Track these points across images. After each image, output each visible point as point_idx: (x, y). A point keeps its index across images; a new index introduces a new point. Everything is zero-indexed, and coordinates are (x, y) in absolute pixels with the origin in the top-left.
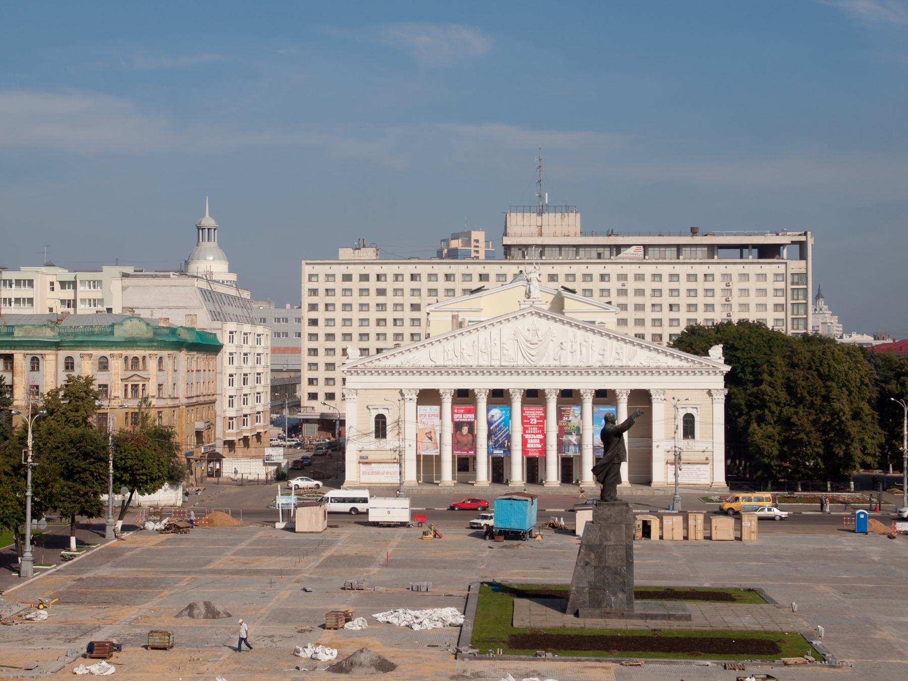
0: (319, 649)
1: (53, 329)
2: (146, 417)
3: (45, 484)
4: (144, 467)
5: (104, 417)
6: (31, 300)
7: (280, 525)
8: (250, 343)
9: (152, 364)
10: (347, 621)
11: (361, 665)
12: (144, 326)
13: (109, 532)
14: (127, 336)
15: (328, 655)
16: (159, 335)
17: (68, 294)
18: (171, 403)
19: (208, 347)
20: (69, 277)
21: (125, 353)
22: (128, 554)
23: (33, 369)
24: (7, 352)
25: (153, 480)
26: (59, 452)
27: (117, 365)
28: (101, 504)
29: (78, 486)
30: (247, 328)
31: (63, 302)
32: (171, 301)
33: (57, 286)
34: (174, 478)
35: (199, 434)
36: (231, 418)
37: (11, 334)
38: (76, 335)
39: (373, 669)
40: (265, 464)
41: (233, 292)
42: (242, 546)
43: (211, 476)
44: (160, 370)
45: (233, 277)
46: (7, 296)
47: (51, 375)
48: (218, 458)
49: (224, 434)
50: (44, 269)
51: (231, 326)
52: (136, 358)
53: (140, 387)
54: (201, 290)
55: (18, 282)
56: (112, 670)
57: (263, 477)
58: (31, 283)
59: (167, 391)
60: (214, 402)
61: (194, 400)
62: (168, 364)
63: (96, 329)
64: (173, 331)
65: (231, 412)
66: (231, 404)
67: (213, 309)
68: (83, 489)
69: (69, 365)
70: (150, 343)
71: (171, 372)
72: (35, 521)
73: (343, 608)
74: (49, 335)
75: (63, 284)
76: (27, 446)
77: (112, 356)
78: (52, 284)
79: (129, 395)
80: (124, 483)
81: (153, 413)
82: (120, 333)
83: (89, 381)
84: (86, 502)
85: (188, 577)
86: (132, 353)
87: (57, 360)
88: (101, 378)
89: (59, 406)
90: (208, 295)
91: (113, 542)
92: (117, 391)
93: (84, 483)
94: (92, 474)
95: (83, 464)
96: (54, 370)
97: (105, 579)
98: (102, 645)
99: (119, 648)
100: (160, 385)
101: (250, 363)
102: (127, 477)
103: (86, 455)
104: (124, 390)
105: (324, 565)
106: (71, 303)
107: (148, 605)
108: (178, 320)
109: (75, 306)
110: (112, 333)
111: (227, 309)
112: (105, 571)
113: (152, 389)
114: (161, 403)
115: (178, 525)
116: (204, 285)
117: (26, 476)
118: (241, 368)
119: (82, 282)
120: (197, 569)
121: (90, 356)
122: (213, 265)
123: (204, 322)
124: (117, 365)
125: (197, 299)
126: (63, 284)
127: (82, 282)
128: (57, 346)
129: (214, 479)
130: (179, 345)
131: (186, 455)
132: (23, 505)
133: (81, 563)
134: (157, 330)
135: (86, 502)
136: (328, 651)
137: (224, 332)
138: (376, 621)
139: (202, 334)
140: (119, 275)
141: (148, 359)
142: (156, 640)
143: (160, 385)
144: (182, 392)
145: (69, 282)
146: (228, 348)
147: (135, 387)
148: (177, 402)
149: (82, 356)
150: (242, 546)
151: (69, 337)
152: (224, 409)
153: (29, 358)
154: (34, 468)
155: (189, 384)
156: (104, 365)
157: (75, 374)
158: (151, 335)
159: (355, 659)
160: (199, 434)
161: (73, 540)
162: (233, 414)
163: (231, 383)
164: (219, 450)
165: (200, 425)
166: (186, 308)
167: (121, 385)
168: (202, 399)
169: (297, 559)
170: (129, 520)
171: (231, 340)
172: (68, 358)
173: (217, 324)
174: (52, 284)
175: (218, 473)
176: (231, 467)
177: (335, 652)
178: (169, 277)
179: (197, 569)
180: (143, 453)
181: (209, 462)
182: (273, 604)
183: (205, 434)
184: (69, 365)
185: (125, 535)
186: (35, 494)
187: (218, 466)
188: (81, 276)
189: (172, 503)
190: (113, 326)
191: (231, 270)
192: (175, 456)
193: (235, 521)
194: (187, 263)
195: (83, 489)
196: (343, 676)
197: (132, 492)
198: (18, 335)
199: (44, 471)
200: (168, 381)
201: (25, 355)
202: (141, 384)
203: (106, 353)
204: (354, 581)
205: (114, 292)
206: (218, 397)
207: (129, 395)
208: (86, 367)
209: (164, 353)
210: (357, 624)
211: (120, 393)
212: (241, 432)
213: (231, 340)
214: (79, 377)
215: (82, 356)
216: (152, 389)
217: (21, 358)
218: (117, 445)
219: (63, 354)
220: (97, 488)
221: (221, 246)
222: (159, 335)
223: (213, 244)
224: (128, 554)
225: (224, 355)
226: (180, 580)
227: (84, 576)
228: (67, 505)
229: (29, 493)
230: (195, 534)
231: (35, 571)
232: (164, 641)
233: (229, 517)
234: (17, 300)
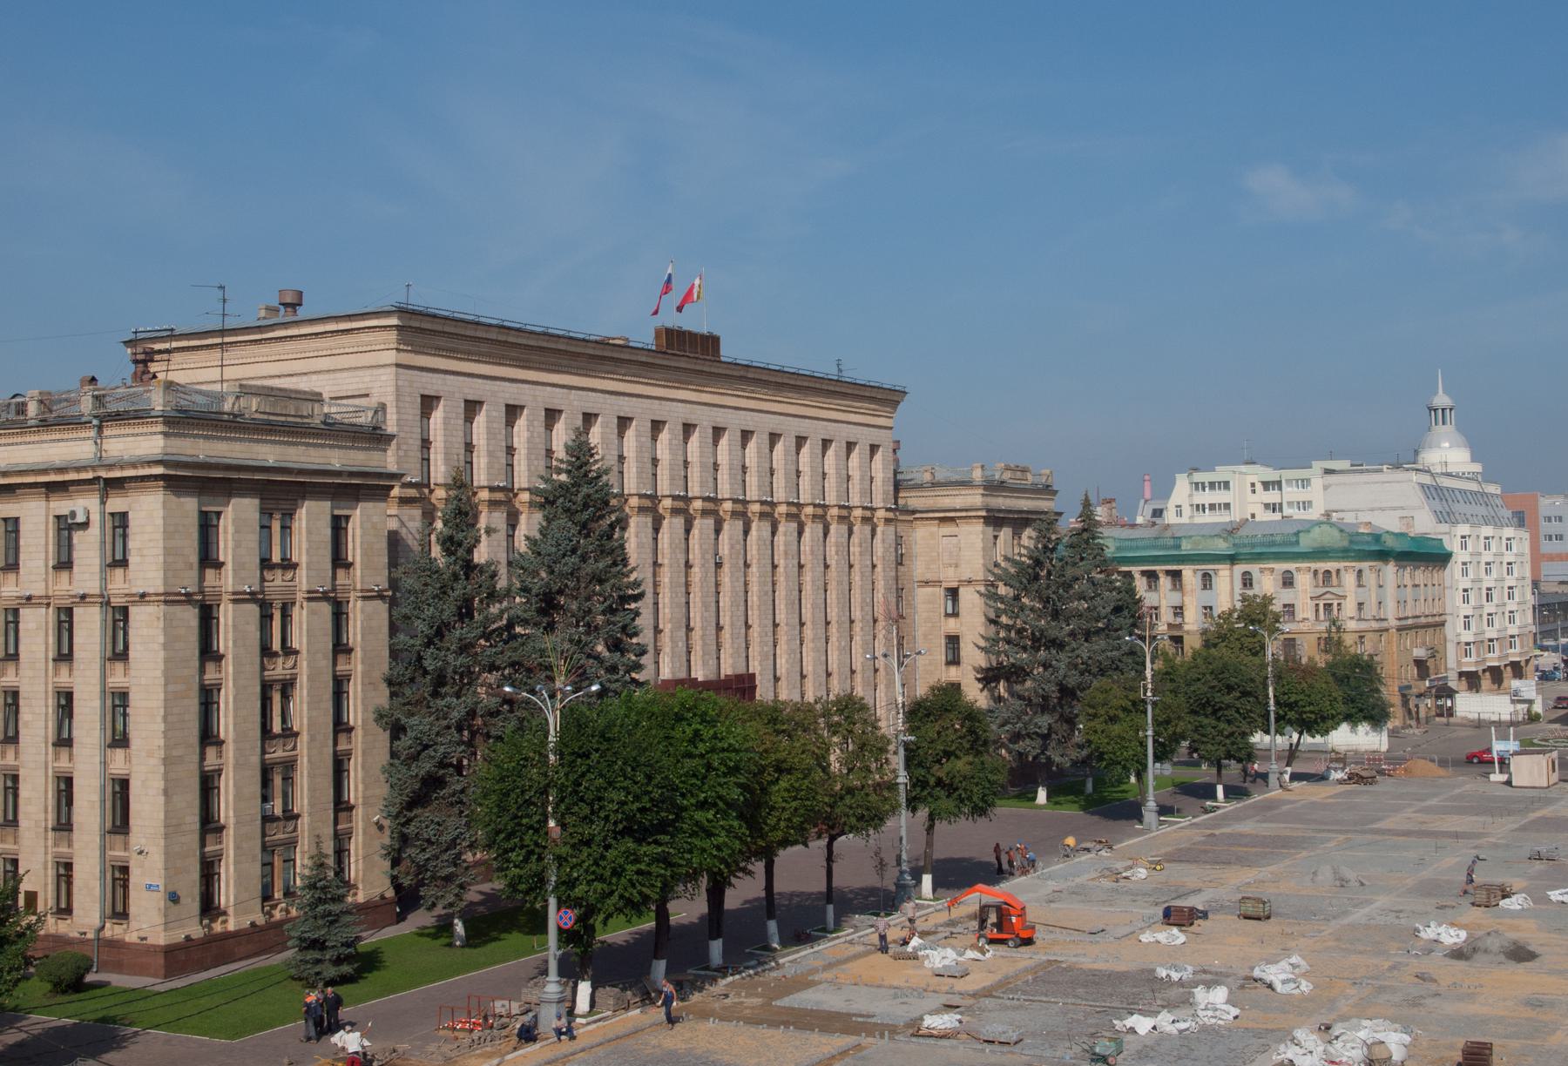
0: (1442, 930)
1: (1225, 540)
2: (1339, 642)
3: (1168, 722)
4: (1311, 704)
5: (1290, 644)
6: (1227, 506)
7: (1497, 777)
8: (1494, 549)
9: (1349, 579)
10: (1504, 897)
11: (1486, 951)
12: (1336, 533)
13: (1273, 779)
14: (1315, 545)
15: (1452, 937)
16: (1357, 543)
17: (1272, 496)
18: (1375, 625)
19: (1431, 557)
20: (1271, 475)
21: (1314, 566)
22: (1285, 808)
23: (1205, 587)
24: (1175, 568)
25: (1324, 719)
26: (1199, 684)
27: (1304, 581)
28: (1251, 746)
29: (1222, 725)
30: (1487, 531)
31: (1267, 506)
32: (1386, 502)
33: (1259, 487)
34: (1375, 716)
35: (1420, 664)
36: (1468, 644)
37: (1178, 547)
38: (1253, 546)
39: (1502, 958)
40: (1513, 702)
41: (1474, 487)
42: (1434, 802)
43: (1441, 715)
44: (1360, 586)
45: (1477, 468)
46: (1200, 502)
47: (1226, 592)
48: (1451, 694)
49: (1459, 663)
50: (1244, 468)
51: (1463, 529)
52: (1328, 572)
53: (1335, 607)
54: (1422, 486)
55: (1212, 485)
56: (1182, 938)
57: (1506, 717)
58: (1226, 485)
59: (1370, 610)
60: (1442, 624)
61: (1410, 622)
62: (1370, 578)
63: (1278, 539)
64: (1377, 538)
65: (1467, 636)
66: (1467, 626)
67: (1439, 508)
68: (1228, 729)
69: (1247, 581)
70: (1345, 554)
71: (1374, 588)
72: (1158, 765)
73: (1498, 880)
74: (1222, 546)
75: (1266, 485)
76: (1145, 679)
77: (1298, 569)
78: (1253, 485)
79: (1322, 617)
80: (1290, 722)
81: (1349, 640)
82: (1306, 543)
83: (1267, 600)
84: (1233, 743)
85: (1341, 837)
86: (1323, 566)
87: (1232, 576)
88: (1283, 597)
89: (1232, 630)
90: (1434, 492)
91: (1276, 793)
92: (1305, 610)
93: (1229, 722)
94: (1238, 711)
95: (1228, 699)
96: (1228, 588)
97: (1242, 835)
98: (1180, 910)
99: (1205, 915)
100: (1360, 604)
101: (1494, 575)
102: (1292, 715)
103: (1230, 688)
104: (1311, 610)
105: (1523, 829)
106: (1274, 507)
107: (1271, 868)
108: (1389, 523)
109: (1281, 510)
110: (1297, 543)
111: (1457, 507)
112: (1247, 827)
113: (1349, 608)
114: (1363, 626)
115: (1365, 771)
116: (1427, 479)
117: (1145, 712)
118: (1480, 581)
119: (1289, 482)
120: (1358, 828)
121: (1272, 570)
122: (1449, 454)
123: (1424, 523)
124: (1304, 581)
125: (1417, 498)
126: (1266, 485)
127: (1289, 482)
128: (1232, 559)
129: (1444, 720)
130: (1383, 555)
131: (1401, 689)
132: (1143, 744)
133: (1225, 817)
134: (1354, 537)
135: (1233, 743)
136: (1452, 932)
137: (1452, 538)
138: (917, 875)
139: (1422, 539)
140: (1321, 472)
141: (1342, 572)
142: (1249, 908)
143: (1360, 604)
144: (1391, 612)
145: (1273, 483)
146: (1460, 556)
147: (1328, 607)
148: (1384, 625)
149: (1262, 571)
150: (1434, 802)
151: (1244, 548)
152: (1456, 631)
153: (1200, 574)
154: (1154, 704)
155: (1401, 603)
156: (1288, 581)
157: (1250, 593)
158: (1345, 543)
159: (1480, 944)
160: (1420, 664)
161: (1220, 789)
162: (1494, 635)
163: (1466, 600)
164: (1453, 684)
165: (1420, 653)
166: (1402, 508)
167: (1311, 604)
168: (1423, 620)
169: (1490, 819)
170: (1299, 767)
171: (1464, 546)
172: (1246, 573)
173: (1444, 527)
174: (1253, 485)
175: (1451, 712)
176: (1468, 705)
177: (1463, 934)
178: (1381, 471)
179: (1358, 828)
180: (1311, 686)
181: (1438, 697)
182: (1426, 874)
183: (1430, 663)
184: (1247, 581)
185: (1295, 784)
186: (1157, 734)
187: (1449, 703)
188: (1287, 474)
189: (1375, 747)
190: (1297, 534)
191: (1474, 460)
192: (1378, 691)
193: (1442, 772)
194: (1416, 453)
195: (1228, 729)
196: (1461, 964)
197: (1301, 733)
198: (1187, 547)
199: (1167, 707)
200: (1369, 601)
201: (1195, 571)
202: (1335, 603)
203: (1291, 566)
204: (1543, 849)
205: (1324, 496)
206: (1448, 618)
207: (1322, 617)
208: (1267, 583)
209: (1365, 565)
210: (1513, 903)
211: (1310, 615)
212: (1484, 660)
213: (1464, 546)
214: (1255, 596)
215: (1262, 571)
216: (1349, 608)
217: (1189, 574)
218: (1278, 677)
219: (1240, 569)
220: (1245, 727)
221: (1459, 429)
222: (1357, 543)
223: (1449, 428)
224: (1285, 808)
225: (1454, 568)
226: (1329, 840)
227: (1217, 832)
228: (1209, 747)
229: (1150, 733)
230: (1384, 785)
231: (1162, 823)
232: (1259, 910)
233: (1434, 766)
234: (1212, 507)
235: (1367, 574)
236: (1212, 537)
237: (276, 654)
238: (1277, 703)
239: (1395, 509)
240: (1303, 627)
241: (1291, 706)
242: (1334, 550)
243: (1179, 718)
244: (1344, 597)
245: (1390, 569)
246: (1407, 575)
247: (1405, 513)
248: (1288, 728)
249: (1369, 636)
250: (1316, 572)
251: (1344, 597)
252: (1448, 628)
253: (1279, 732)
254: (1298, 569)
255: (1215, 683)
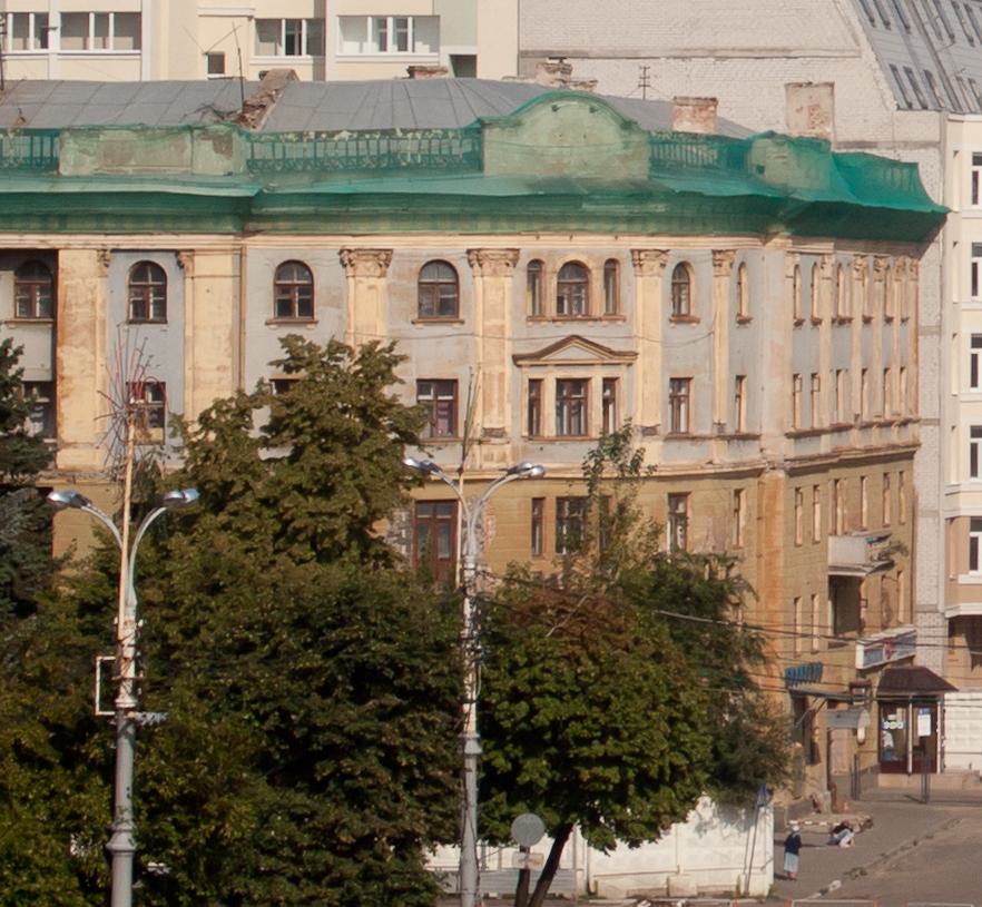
1: (223, 145)
2: (620, 519)
3: (193, 802)
4: (609, 732)
9: (646, 294)
12: (610, 134)
14: (539, 172)
16: (676, 169)
18: (723, 456)
21: (531, 244)
23: (139, 314)
24: (32, 241)
25: (647, 784)
27: (494, 297)
29: (331, 812)
35: (843, 589)
38: (321, 168)
44: (680, 318)
47: (220, 339)
52: (576, 268)
60: (907, 454)
61: (824, 445)
62: (712, 293)
63: (409, 146)
64: (734, 152)
67: (903, 60)
68: (354, 824)
69: (295, 295)
70: (634, 204)
71: (724, 326)
74: (209, 168)
76: (113, 641)
79: (549, 424)
80: (528, 796)
81: (649, 501)
82: (508, 162)
83: (378, 364)
84: (367, 876)
86: (559, 246)
87: (240, 276)
88: (428, 352)
89: (250, 469)
92: (496, 405)
93: (357, 799)
94: (389, 760)
95: (352, 717)
100: (678, 383)
102: (537, 770)
108: (755, 105)
109: (317, 47)
110: (475, 162)
113: (643, 400)
114: (685, 458)
117: (108, 770)
121: (384, 258)
128: (244, 215)
129: (909, 783)
130: (760, 214)
134: (664, 149)
135: (367, 876)
139: (855, 164)
141: (626, 270)
143: (678, 383)
144: (770, 411)
147: (573, 389)
148: (749, 455)
149: (347, 259)
153: (123, 265)
154: (143, 735)
155: (802, 379)
156: (439, 297)
158: (638, 170)
160: (843, 589)
165: (848, 552)
166: (786, 54)
167: (515, 381)
168: (856, 441)
180: (608, 670)
181: (887, 707)
183: (869, 590)
184: (295, 295)
186: (149, 844)
189: (728, 880)
190: (477, 130)
192: (743, 681)
195: (354, 824)
197: (560, 835)
198: (78, 167)
199: (186, 746)
201: (105, 256)
202: (597, 377)
203: (449, 244)
206: (924, 434)
207: (549, 424)
208: (363, 306)
209: (697, 247)
214: (336, 348)
215: (347, 259)
216: (643, 400)
217: (88, 269)
219: (268, 250)
220: (413, 818)
222: (676, 169)
229: (123, 841)
235: (703, 277)
236: (171, 132)
237: (168, 659)
238: (488, 728)
239: (759, 55)
240: (487, 460)
241: (531, 740)
242: (598, 193)
243: (233, 786)
244: (628, 358)
245: (774, 257)
246: (824, 288)
247: (797, 71)
248: (527, 820)
249: (701, 494)
250: (535, 267)
251: (628, 358)
252: (922, 470)
253: (493, 834)
254: (475, 257)
255: (314, 659)
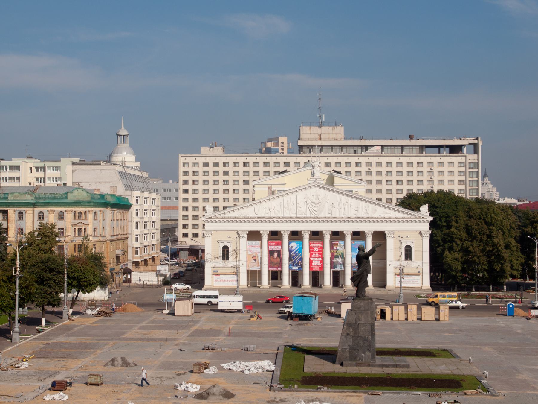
0: (189, 385)
1: (31, 195)
2: (87, 247)
3: (27, 287)
4: (85, 277)
5: (61, 248)
6: (18, 178)
7: (166, 311)
8: (148, 203)
9: (90, 216)
10: (206, 368)
11: (214, 394)
12: (85, 194)
13: (65, 315)
14: (75, 199)
15: (194, 389)
16: (94, 199)
17: (40, 175)
18: (101, 239)
19: (123, 206)
20: (41, 164)
21: (74, 209)
22: (76, 329)
23: (19, 219)
24: (4, 209)
25: (90, 285)
26: (35, 268)
27: (69, 217)
28: (60, 299)
29: (46, 289)
30: (146, 195)
31: (37, 179)
32: (101, 179)
33: (34, 169)
34: (103, 284)
35: (118, 257)
36: (137, 248)
37: (7, 198)
38: (45, 199)
39: (221, 397)
40: (157, 275)
41: (138, 173)
42: (143, 324)
43: (125, 282)
44: (95, 219)
45: (138, 164)
46: (4, 176)
47: (30, 222)
48: (129, 272)
49: (133, 257)
50: (26, 160)
51: (137, 193)
52: (81, 212)
53: (83, 230)
54: (119, 172)
55: (11, 167)
56: (67, 397)
57: (156, 283)
58: (18, 168)
59: (99, 232)
60: (127, 239)
61: (115, 237)
62: (99, 216)
63: (57, 195)
64: (103, 196)
65: (137, 245)
66: (137, 240)
67: (126, 183)
68: (49, 290)
69: (41, 216)
70: (89, 204)
71: (101, 221)
72: (21, 309)
73: (203, 361)
74: (29, 198)
75: (37, 169)
76: (16, 265)
77: (66, 211)
78: (31, 168)
79: (77, 234)
80: (74, 286)
81: (91, 245)
82: (71, 198)
83: (53, 226)
84: (51, 298)
85: (112, 343)
86: (78, 209)
87: (34, 214)
88: (60, 224)
89: (35, 241)
90: (123, 175)
91: (67, 322)
92: (69, 232)
93: (50, 287)
94: (54, 281)
95: (49, 275)
96: (32, 219)
97: (62, 343)
98: (60, 382)
99: (70, 384)
100: (95, 228)
101: (148, 216)
102: (75, 283)
103: (51, 270)
104: (74, 232)
105: (192, 335)
106: (42, 180)
107: (88, 359)
108: (105, 190)
109: (44, 182)
110: (66, 198)
111: (134, 183)
112: (62, 339)
113: (90, 231)
114: (96, 239)
115: (105, 311)
116: (121, 169)
117: (15, 283)
118: (143, 218)
119: (49, 167)
120: (117, 338)
121: (54, 211)
122: (126, 157)
123: (121, 191)
124: (69, 217)
125: (117, 178)
126: (37, 169)
127: (49, 167)
128: (34, 205)
129: (127, 284)
130: (106, 205)
131: (110, 270)
132: (14, 299)
133: (48, 334)
134: (93, 196)
135: (51, 298)
136: (194, 386)
137: (132, 197)
139: (120, 198)
140: (71, 163)
141: (87, 213)
142: (93, 380)
143: (95, 228)
144: (108, 233)
145: (41, 168)
146: (135, 206)
147: (80, 230)
148: (105, 239)
149: (48, 211)
150: (143, 324)
151: (41, 200)
152: (132, 243)
153: (17, 212)
154: (20, 278)
155: (112, 228)
156: (61, 217)
157: (44, 222)
158: (89, 199)
159: (210, 391)
160: (118, 257)
161: (43, 320)
162: (138, 246)
163: (137, 227)
164: (130, 267)
165: (118, 252)
166: (110, 183)
167: (72, 228)
168: (119, 237)
169: (176, 331)
170: (76, 309)
171: (137, 202)
172: (40, 212)
173: (129, 192)
174: (31, 168)
175: (129, 281)
176: (137, 277)
177: (199, 387)
178: (100, 164)
179: (117, 338)
180: (85, 269)
181: (124, 274)
182: (162, 359)
183: (121, 258)
184: (41, 216)
185: (74, 317)
186: (21, 293)
187: (129, 277)
188: (48, 164)
189: (102, 298)
190: (67, 193)
191: (137, 160)
192: (104, 270)
193: (139, 309)
194: (111, 156)
195: (49, 290)
196: (203, 401)
197: (78, 292)
198: (11, 198)
199: (26, 279)
200: (99, 226)
201: (15, 211)
202: (83, 228)
203: (63, 209)
204: (210, 345)
205: (68, 173)
206: (129, 236)
207: (77, 234)
208: (51, 218)
209: (97, 210)
210: (211, 370)
211: (71, 233)
212: (143, 256)
213: (137, 202)
214: (47, 224)
215: (48, 211)
216: (90, 231)
217: (12, 213)
218: (69, 264)
219: (37, 210)
220: (58, 289)
221: (131, 146)
222: (94, 199)
223: (126, 145)
224: (76, 329)
225: (133, 211)
226: (107, 344)
227: (50, 342)
228: (40, 299)
229: (17, 293)
230: (116, 317)
231: (21, 339)
232: (97, 381)
233: (135, 306)
234: (10, 178)
